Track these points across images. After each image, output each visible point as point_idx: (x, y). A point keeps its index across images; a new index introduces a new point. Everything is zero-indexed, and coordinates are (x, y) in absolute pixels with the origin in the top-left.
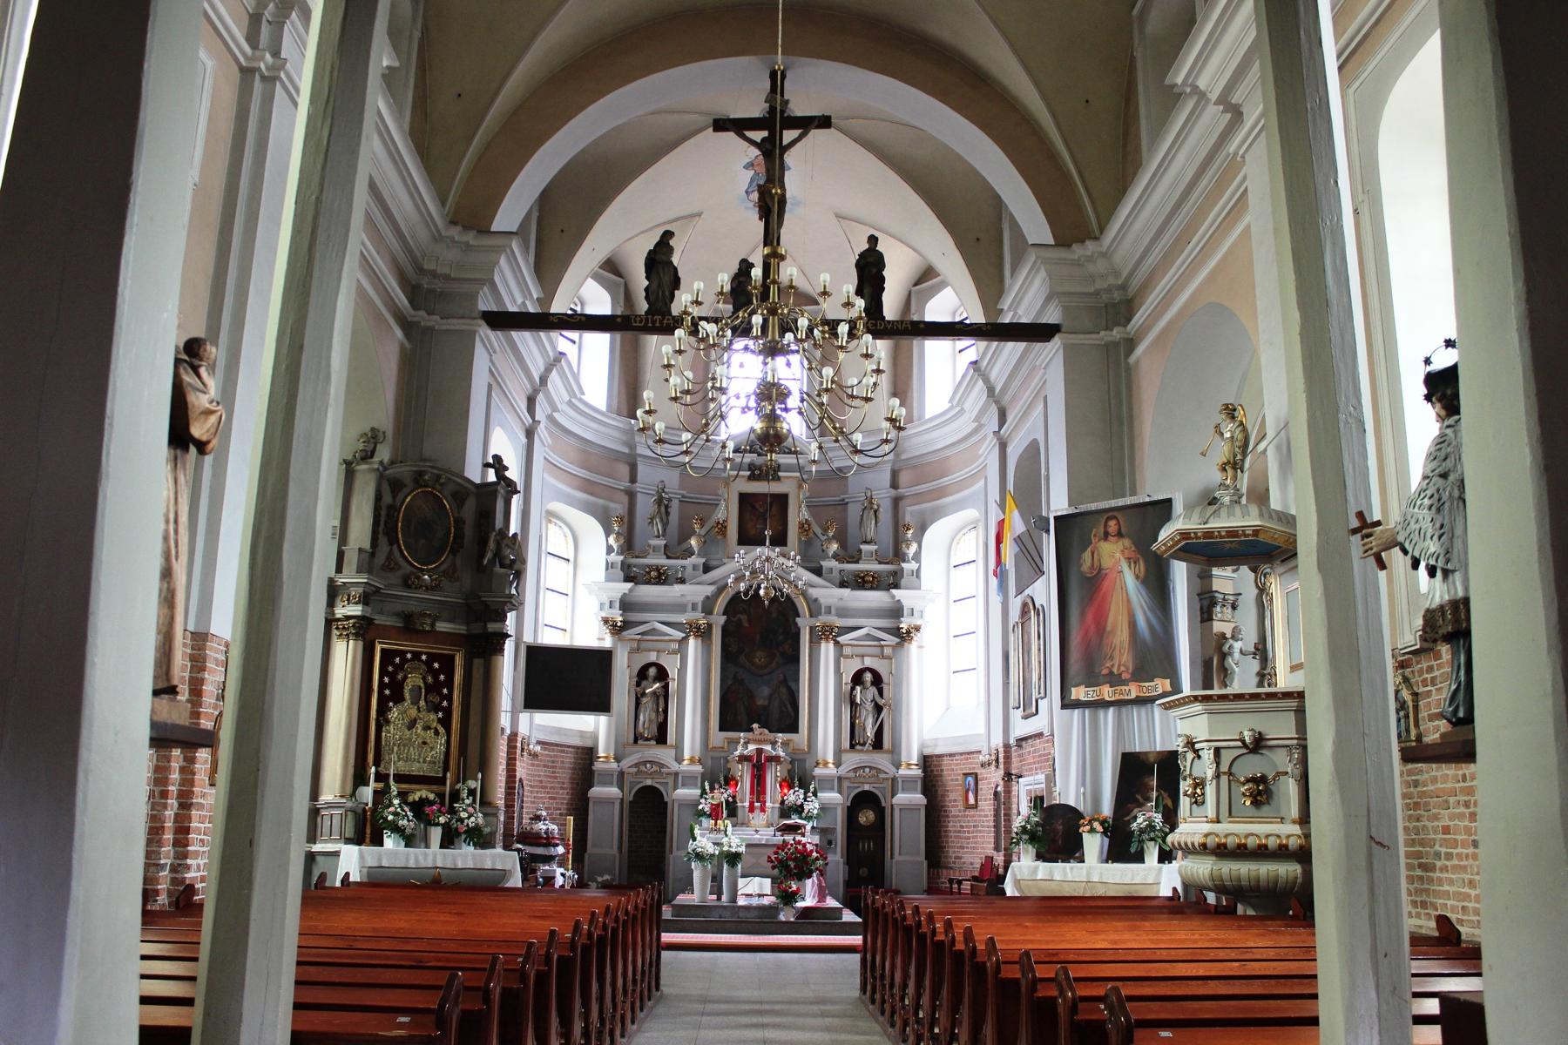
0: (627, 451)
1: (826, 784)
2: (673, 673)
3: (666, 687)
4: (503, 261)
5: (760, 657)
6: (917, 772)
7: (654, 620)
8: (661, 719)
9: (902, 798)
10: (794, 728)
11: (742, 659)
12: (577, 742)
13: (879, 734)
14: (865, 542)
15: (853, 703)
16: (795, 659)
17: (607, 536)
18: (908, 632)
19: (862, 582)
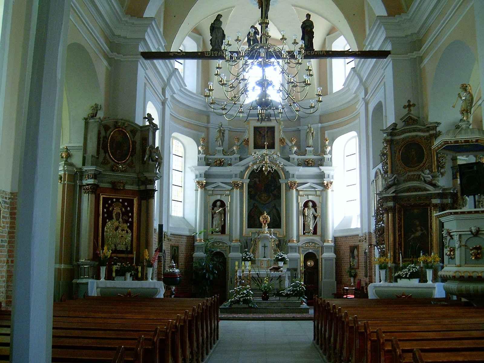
1: (294, 249)
2: (228, 204)
3: (225, 210)
5: (264, 196)
11: (257, 197)
15: (304, 215)
16: (279, 197)
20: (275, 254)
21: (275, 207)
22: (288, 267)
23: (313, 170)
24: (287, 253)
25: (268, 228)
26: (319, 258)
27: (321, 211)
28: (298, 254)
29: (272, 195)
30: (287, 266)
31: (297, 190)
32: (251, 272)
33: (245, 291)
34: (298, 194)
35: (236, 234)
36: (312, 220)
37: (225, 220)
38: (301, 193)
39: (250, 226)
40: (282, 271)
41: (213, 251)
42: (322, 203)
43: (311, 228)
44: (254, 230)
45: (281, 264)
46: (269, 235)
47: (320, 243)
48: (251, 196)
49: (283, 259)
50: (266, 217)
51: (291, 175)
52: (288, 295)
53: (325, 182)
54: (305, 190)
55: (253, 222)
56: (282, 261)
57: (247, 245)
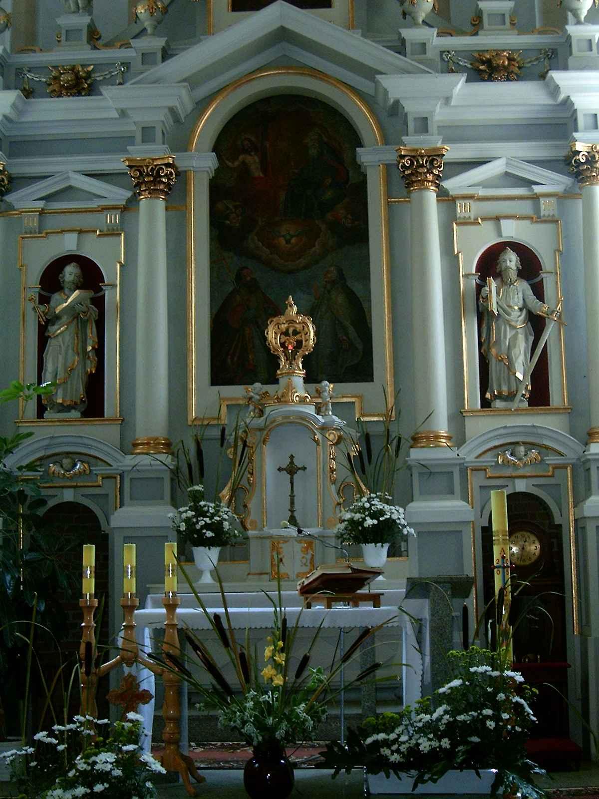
1: (440, 479)
2: (112, 273)
3: (99, 302)
5: (288, 234)
7: (69, 170)
8: (91, 368)
11: (253, 241)
15: (483, 316)
16: (359, 235)
19: (485, 69)
20: (345, 504)
21: (340, 281)
22: (415, 574)
23: (517, 98)
24: (405, 500)
25: (307, 380)
26: (567, 518)
27: (567, 292)
28: (465, 503)
29: (323, 227)
30: (409, 567)
31: (443, 195)
32: (179, 611)
33: (105, 760)
34: (450, 219)
35: (152, 412)
36: (521, 337)
37: (100, 351)
38: (464, 209)
39: (220, 374)
40: (376, 599)
41: (42, 502)
42: (563, 253)
43: (520, 376)
44: (236, 392)
45: (375, 555)
46: (311, 410)
47: (564, 444)
48: (224, 236)
49: (386, 532)
50: (293, 327)
51: (411, 125)
52: (419, 763)
53: (579, 146)
54: (482, 192)
55: (237, 356)
56: (383, 542)
57: (204, 467)
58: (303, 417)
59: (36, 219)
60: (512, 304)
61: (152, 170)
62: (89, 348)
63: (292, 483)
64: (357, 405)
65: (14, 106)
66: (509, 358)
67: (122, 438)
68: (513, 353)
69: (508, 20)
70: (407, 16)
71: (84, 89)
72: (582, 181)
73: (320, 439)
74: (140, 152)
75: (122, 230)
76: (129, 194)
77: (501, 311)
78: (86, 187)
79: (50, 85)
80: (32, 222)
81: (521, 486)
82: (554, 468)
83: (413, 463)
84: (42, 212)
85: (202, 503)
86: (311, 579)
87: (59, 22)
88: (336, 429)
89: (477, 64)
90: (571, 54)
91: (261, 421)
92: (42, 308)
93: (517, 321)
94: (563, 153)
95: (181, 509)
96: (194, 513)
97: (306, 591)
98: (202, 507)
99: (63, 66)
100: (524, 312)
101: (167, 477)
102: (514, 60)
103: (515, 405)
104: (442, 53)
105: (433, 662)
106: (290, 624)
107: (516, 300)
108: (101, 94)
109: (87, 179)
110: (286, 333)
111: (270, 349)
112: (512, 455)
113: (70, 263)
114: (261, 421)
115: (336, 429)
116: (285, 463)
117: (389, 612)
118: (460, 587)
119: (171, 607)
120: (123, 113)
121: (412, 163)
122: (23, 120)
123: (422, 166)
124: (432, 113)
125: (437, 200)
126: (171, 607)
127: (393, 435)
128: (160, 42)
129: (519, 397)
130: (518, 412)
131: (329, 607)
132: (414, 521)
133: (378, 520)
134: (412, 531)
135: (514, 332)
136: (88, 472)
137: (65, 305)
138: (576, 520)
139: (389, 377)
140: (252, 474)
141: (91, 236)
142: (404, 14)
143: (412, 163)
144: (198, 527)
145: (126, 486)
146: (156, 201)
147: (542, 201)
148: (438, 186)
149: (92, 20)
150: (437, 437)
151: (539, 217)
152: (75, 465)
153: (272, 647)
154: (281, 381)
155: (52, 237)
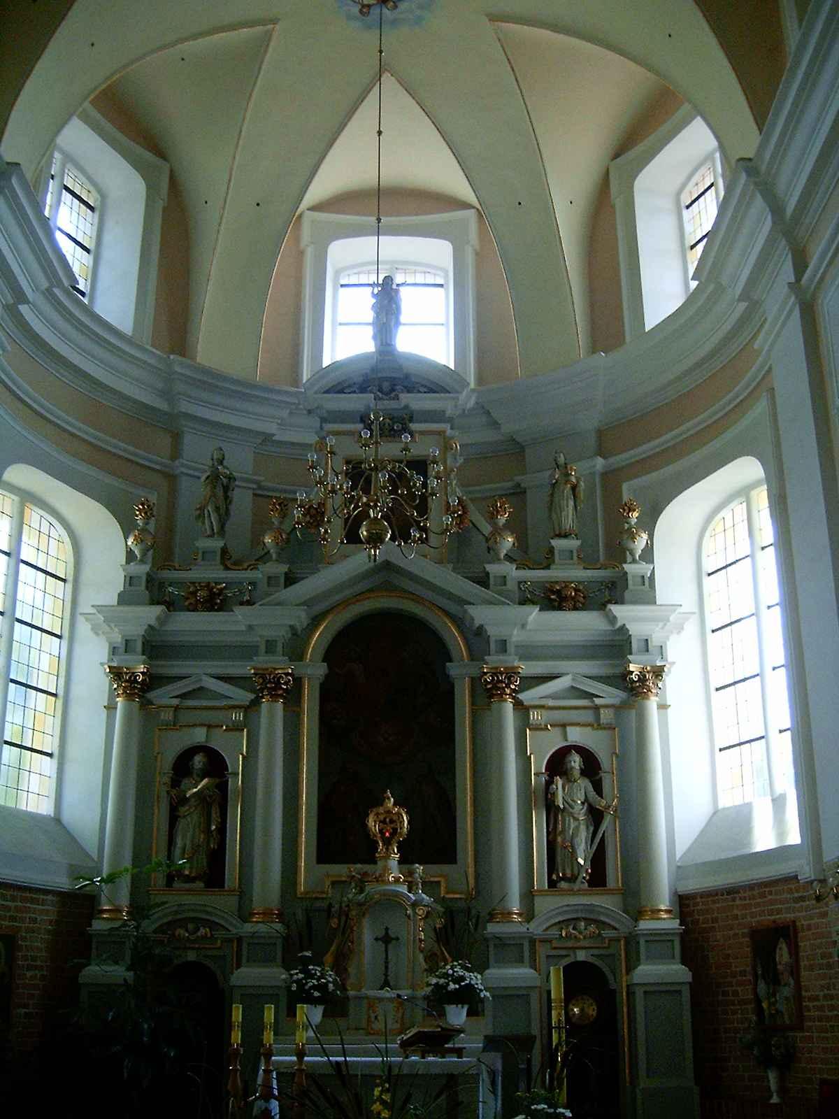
0: (163, 406)
1: (513, 949)
3: (223, 787)
4: (14, 181)
6: (670, 924)
7: (201, 673)
9: (650, 971)
10: (453, 860)
12: (62, 882)
13: (598, 860)
14: (559, 536)
15: (552, 810)
17: (126, 538)
18: (643, 679)
19: (556, 598)
20: (431, 971)
22: (489, 1032)
23: (580, 624)
25: (400, 862)
28: (532, 971)
30: (485, 1026)
31: (518, 704)
34: (524, 724)
36: (583, 827)
37: (222, 830)
38: (535, 716)
39: (325, 854)
40: (459, 1052)
42: (621, 758)
43: (582, 862)
44: (340, 870)
46: (403, 889)
48: (329, 733)
49: (467, 996)
50: (392, 815)
51: (493, 646)
53: (632, 667)
54: (551, 703)
55: (342, 838)
57: (314, 933)
58: (397, 894)
59: (171, 713)
60: (575, 799)
61: (274, 678)
62: (214, 827)
63: (386, 951)
64: (443, 884)
65: (158, 618)
66: (573, 847)
67: (240, 908)
68: (577, 840)
69: (575, 554)
70: (491, 551)
71: (216, 604)
72: (636, 695)
73: (412, 915)
74: (262, 661)
75: (245, 726)
76: (253, 696)
77: (567, 806)
78: (213, 688)
79: (188, 598)
80: (167, 716)
81: (581, 956)
82: (610, 941)
83: (489, 936)
84: (177, 708)
85: (311, 967)
86: (409, 1035)
87: (197, 545)
88: (425, 906)
89: (549, 594)
90: (627, 588)
91: (361, 897)
92: (174, 792)
93: (579, 814)
94: (618, 671)
95: (292, 972)
96: (303, 976)
97: (404, 1044)
98: (310, 970)
99: (199, 583)
100: (586, 804)
101: (279, 942)
102: (579, 591)
103: (577, 886)
104: (520, 583)
105: (503, 1105)
106: (395, 1071)
107: (579, 795)
108: (232, 611)
109: (221, 683)
110: (383, 822)
111: (370, 835)
112: (574, 929)
113: (199, 753)
114: (361, 897)
115: (425, 906)
116: (381, 933)
117: (470, 1062)
118: (525, 1042)
119: (301, 1054)
120: (250, 627)
121: (493, 678)
122: (164, 628)
123: (502, 682)
124: (511, 636)
125: (514, 709)
126: (301, 1054)
127: (473, 912)
128: (284, 568)
129: (580, 878)
130: (579, 893)
131: (423, 1057)
132: (490, 986)
133: (459, 985)
134: (488, 994)
135: (576, 823)
136: (209, 935)
137: (195, 790)
138: (628, 986)
139: (470, 860)
140: (352, 942)
141: (217, 731)
142: (489, 549)
143: (493, 678)
144: (307, 987)
145: (243, 950)
146: (276, 704)
147: (602, 711)
148: (514, 698)
149: (225, 544)
150: (510, 913)
151: (599, 725)
152: (199, 929)
153: (380, 1089)
154: (379, 862)
155: (185, 729)
